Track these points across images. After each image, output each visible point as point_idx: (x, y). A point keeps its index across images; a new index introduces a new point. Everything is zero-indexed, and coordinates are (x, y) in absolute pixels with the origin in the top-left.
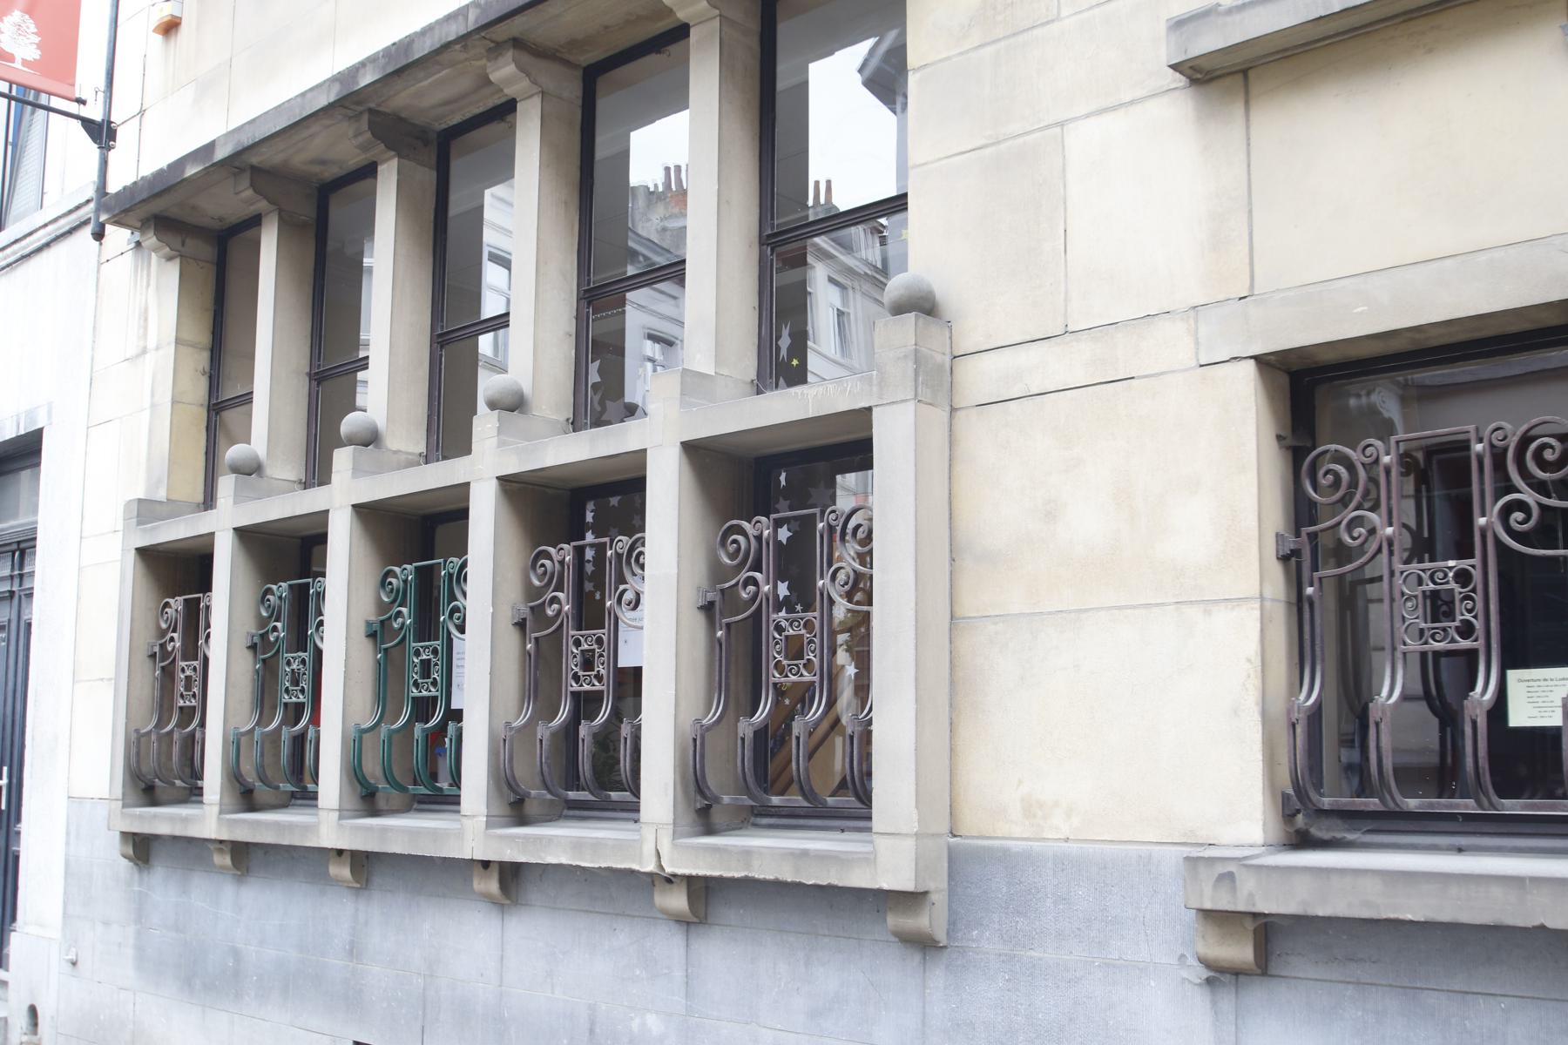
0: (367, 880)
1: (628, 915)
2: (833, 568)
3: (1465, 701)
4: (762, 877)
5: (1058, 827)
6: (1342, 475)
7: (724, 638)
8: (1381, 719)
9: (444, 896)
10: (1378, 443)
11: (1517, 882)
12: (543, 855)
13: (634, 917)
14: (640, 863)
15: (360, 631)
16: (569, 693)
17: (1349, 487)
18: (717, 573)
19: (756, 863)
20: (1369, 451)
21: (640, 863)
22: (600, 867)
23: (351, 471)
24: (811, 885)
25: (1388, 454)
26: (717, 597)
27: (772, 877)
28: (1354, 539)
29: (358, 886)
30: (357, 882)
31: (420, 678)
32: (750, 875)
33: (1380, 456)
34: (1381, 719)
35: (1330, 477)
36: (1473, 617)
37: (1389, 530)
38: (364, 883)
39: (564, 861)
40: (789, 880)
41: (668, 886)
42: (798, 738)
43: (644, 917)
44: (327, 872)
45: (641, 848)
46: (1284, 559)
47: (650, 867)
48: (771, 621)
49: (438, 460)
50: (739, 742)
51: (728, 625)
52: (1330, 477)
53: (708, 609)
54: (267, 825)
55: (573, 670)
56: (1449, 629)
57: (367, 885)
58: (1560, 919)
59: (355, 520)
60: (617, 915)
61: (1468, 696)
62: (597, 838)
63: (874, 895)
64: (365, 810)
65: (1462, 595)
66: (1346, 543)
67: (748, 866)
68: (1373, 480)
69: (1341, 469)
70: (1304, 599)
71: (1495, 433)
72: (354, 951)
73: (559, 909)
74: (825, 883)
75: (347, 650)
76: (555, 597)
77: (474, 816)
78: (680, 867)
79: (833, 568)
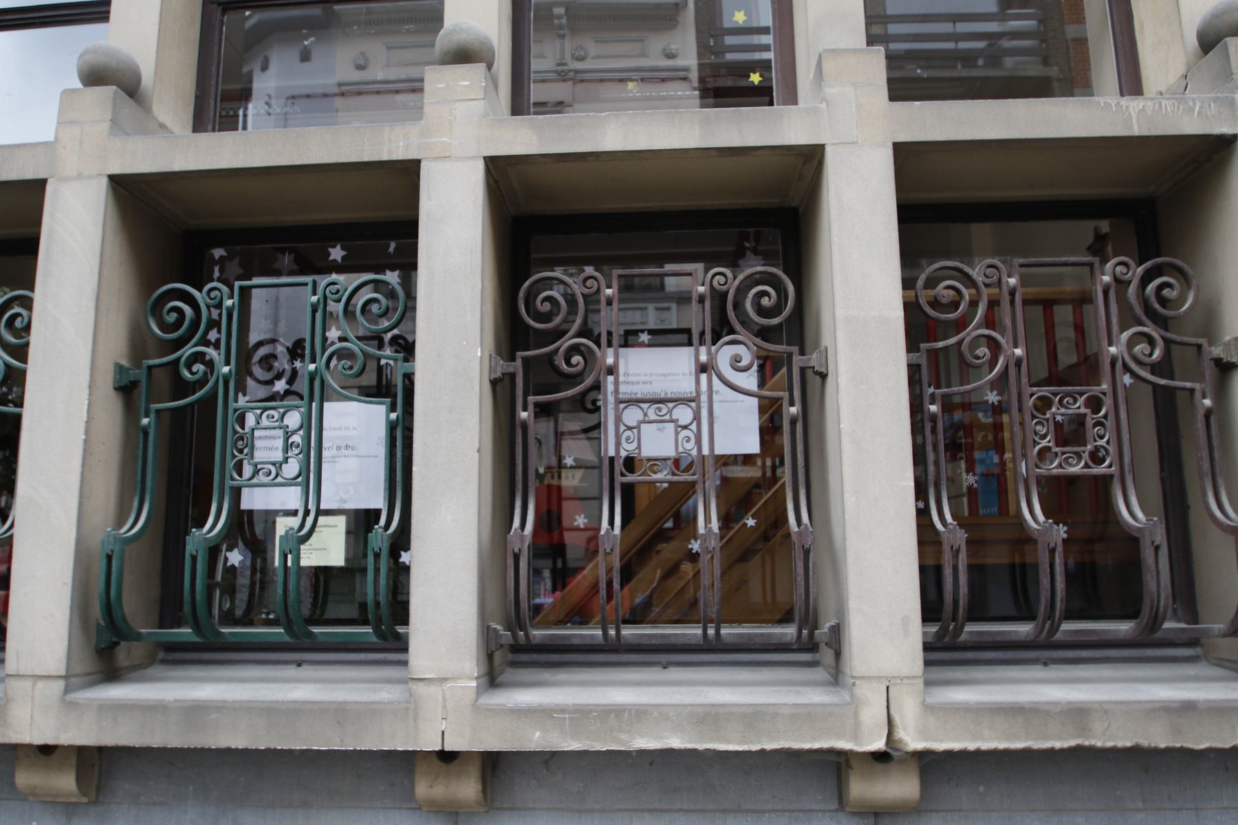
0: (99, 789)
1: (748, 811)
2: (327, 354)
3: (370, 534)
4: (1109, 744)
6: (186, 313)
7: (152, 425)
8: (380, 549)
9: (306, 805)
10: (225, 289)
12: (623, 737)
13: (764, 812)
14: (856, 738)
15: (107, 380)
16: (227, 491)
17: (569, 313)
18: (139, 344)
19: (1097, 726)
20: (213, 294)
21: (856, 738)
22: (763, 751)
23: (109, 123)
24: (756, 752)
25: (609, 287)
26: (142, 375)
27: (1129, 744)
28: (192, 373)
29: (85, 800)
30: (84, 795)
31: (1057, 445)
32: (1087, 743)
33: (601, 287)
34: (197, 552)
35: (174, 315)
36: (236, 456)
37: (226, 369)
38: (93, 793)
39: (676, 743)
40: (1163, 746)
41: (879, 767)
42: (377, 556)
43: (785, 811)
44: (12, 785)
45: (856, 715)
46: (494, 383)
47: (879, 744)
48: (230, 411)
49: (214, 130)
50: (510, 561)
51: (158, 411)
52: (174, 315)
53: (126, 389)
54: (159, 708)
55: (235, 456)
56: (1082, 454)
57: (97, 797)
58: (1226, 740)
59: (111, 200)
60: (724, 811)
61: (373, 528)
62: (89, 699)
63: (546, 762)
64: (101, 672)
65: (1094, 421)
66: (188, 380)
67: (1083, 730)
68: (993, 304)
69: (188, 310)
70: (518, 423)
71: (328, 289)
73: (592, 811)
74: (1228, 745)
75: (89, 405)
76: (203, 354)
77: (444, 680)
78: (942, 741)
79: (327, 354)
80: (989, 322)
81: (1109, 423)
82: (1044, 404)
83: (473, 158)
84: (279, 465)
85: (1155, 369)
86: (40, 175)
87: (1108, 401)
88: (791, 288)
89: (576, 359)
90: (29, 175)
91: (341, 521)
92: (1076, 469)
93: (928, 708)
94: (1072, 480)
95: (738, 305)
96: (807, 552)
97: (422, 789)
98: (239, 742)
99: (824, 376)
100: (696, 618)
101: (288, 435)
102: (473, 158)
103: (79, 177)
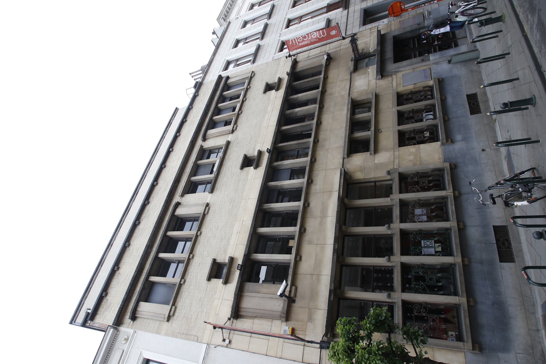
4: (458, 235)
5: (441, 156)
11: (441, 134)
39: (454, 207)
47: (452, 193)
54: (456, 248)
69: (413, 251)
72: (482, 263)
80: (414, 188)
81: (433, 316)
82: (428, 282)
83: (401, 294)
84: (430, 242)
85: (413, 113)
86: (400, 263)
87: (430, 316)
88: (415, 305)
89: (425, 328)
90: (399, 230)
91: (436, 244)
92: (427, 182)
93: (449, 190)
94: (428, 182)
95: (417, 310)
96: (446, 306)
97: (472, 304)
98: (458, 240)
99: (426, 302)
100: (435, 129)
101: (427, 242)
102: (401, 294)
103: (400, 258)
